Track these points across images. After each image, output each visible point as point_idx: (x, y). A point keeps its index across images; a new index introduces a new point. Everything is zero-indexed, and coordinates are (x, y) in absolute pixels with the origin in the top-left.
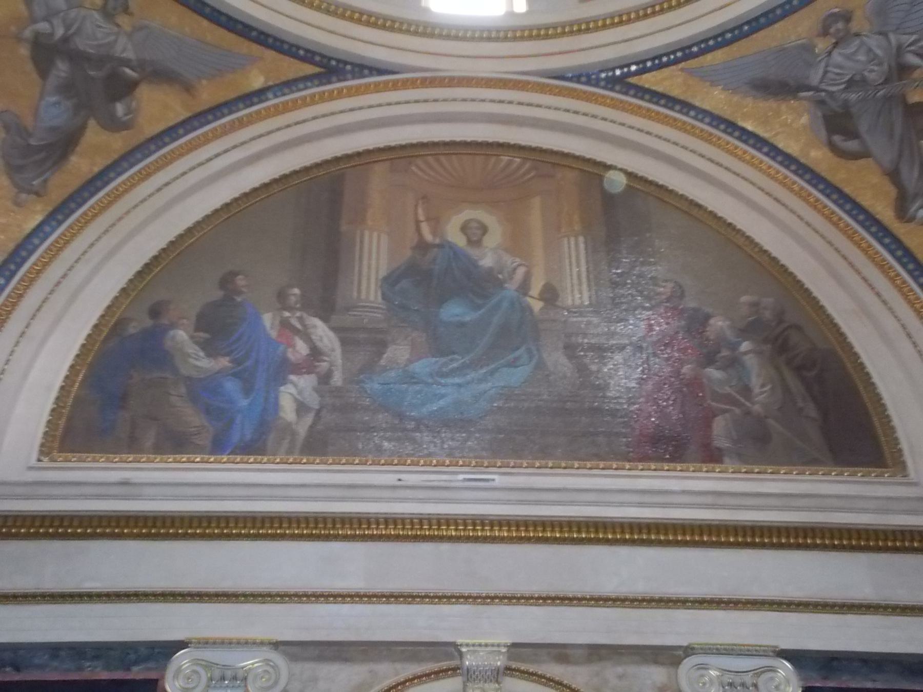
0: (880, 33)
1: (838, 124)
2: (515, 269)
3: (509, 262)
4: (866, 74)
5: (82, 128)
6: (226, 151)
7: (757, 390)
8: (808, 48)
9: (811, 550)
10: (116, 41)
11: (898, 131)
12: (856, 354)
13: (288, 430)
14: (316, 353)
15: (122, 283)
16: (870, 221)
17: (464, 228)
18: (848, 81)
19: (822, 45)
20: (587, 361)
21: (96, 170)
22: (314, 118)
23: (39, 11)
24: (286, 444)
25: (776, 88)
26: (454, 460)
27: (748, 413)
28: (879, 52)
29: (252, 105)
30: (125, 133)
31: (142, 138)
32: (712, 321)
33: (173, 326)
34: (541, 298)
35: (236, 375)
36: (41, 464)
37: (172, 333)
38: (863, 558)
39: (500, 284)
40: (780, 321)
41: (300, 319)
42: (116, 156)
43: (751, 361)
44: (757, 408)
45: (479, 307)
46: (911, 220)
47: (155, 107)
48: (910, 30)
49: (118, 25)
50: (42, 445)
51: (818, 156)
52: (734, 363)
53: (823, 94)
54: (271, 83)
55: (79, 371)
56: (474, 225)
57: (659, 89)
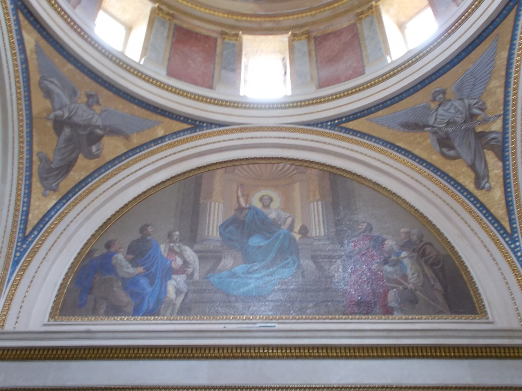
0: (460, 99)
1: (444, 143)
2: (286, 219)
3: (283, 216)
4: (455, 118)
5: (76, 159)
6: (145, 166)
7: (410, 277)
8: (427, 108)
9: (403, 358)
10: (93, 117)
11: (473, 145)
12: (459, 256)
13: (172, 303)
14: (186, 263)
15: (93, 232)
16: (463, 190)
17: (261, 199)
18: (448, 122)
19: (434, 106)
20: (323, 264)
21: (82, 178)
22: (187, 149)
23: (57, 106)
24: (169, 312)
25: (414, 127)
26: (321, 317)
27: (406, 288)
28: (460, 108)
29: (158, 144)
30: (96, 160)
31: (104, 162)
32: (386, 242)
33: (116, 252)
34: (300, 232)
35: (146, 276)
36: (49, 323)
37: (116, 256)
38: (465, 363)
39: (279, 227)
40: (421, 241)
41: (179, 247)
42: (91, 171)
43: (407, 262)
44: (410, 286)
45: (269, 238)
46: (483, 188)
47: (111, 147)
48: (474, 97)
49: (94, 110)
50: (51, 313)
51: (436, 159)
52: (398, 262)
53: (436, 129)
54: (167, 134)
55: (70, 277)
56: (266, 197)
57: (355, 128)
